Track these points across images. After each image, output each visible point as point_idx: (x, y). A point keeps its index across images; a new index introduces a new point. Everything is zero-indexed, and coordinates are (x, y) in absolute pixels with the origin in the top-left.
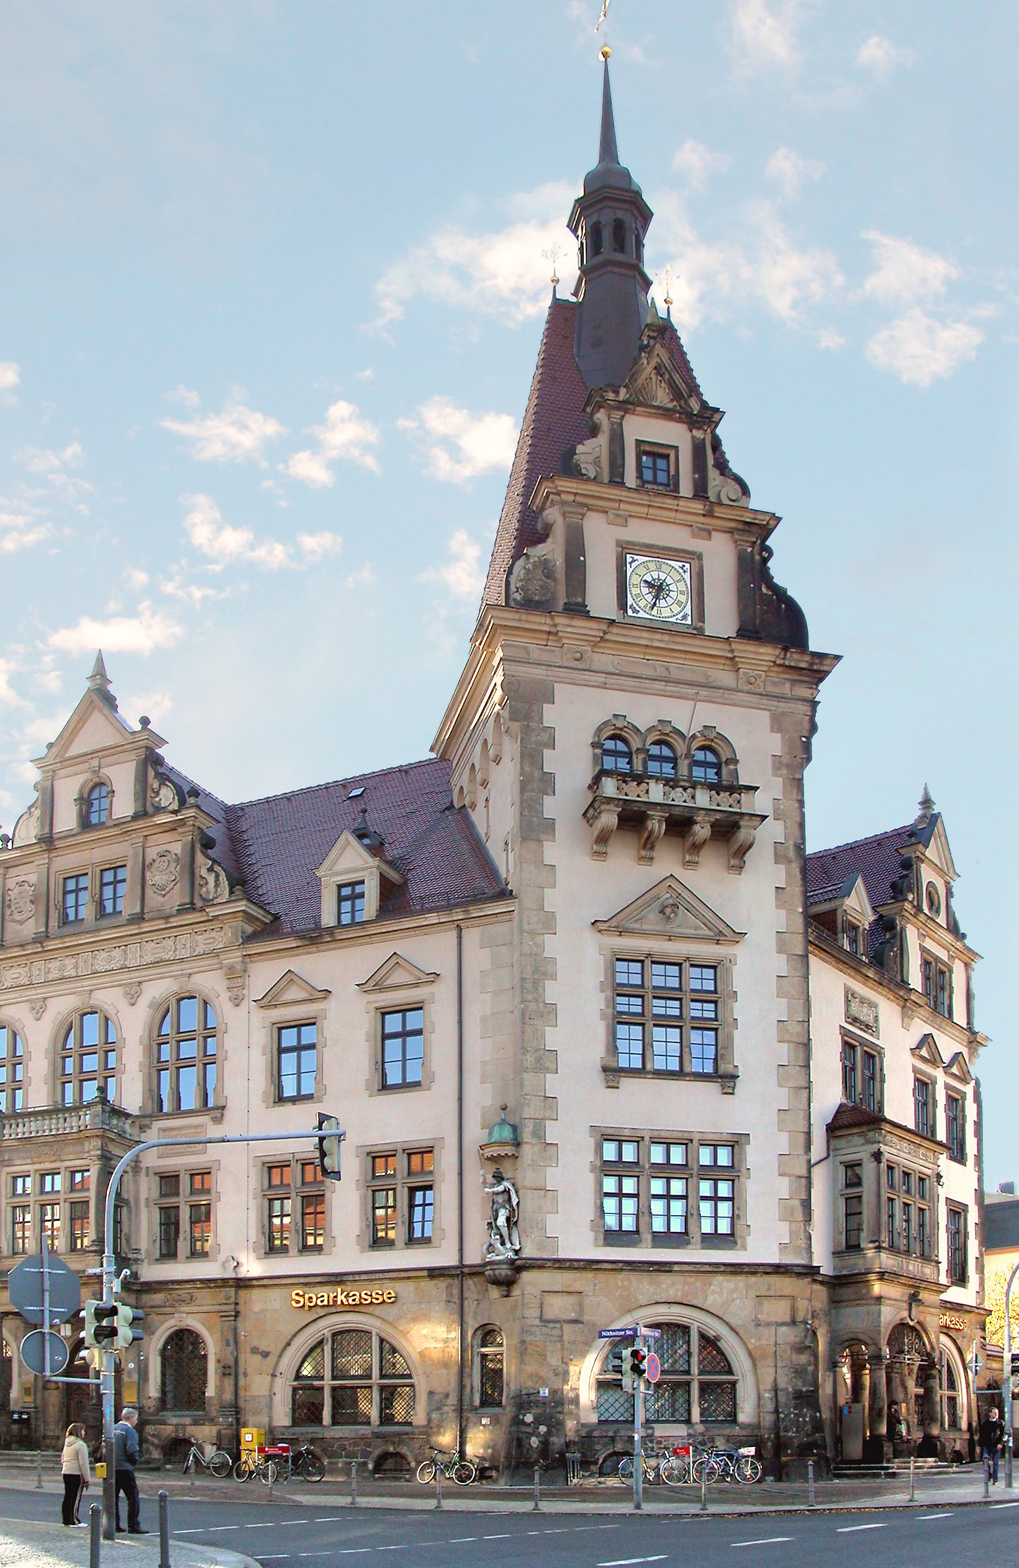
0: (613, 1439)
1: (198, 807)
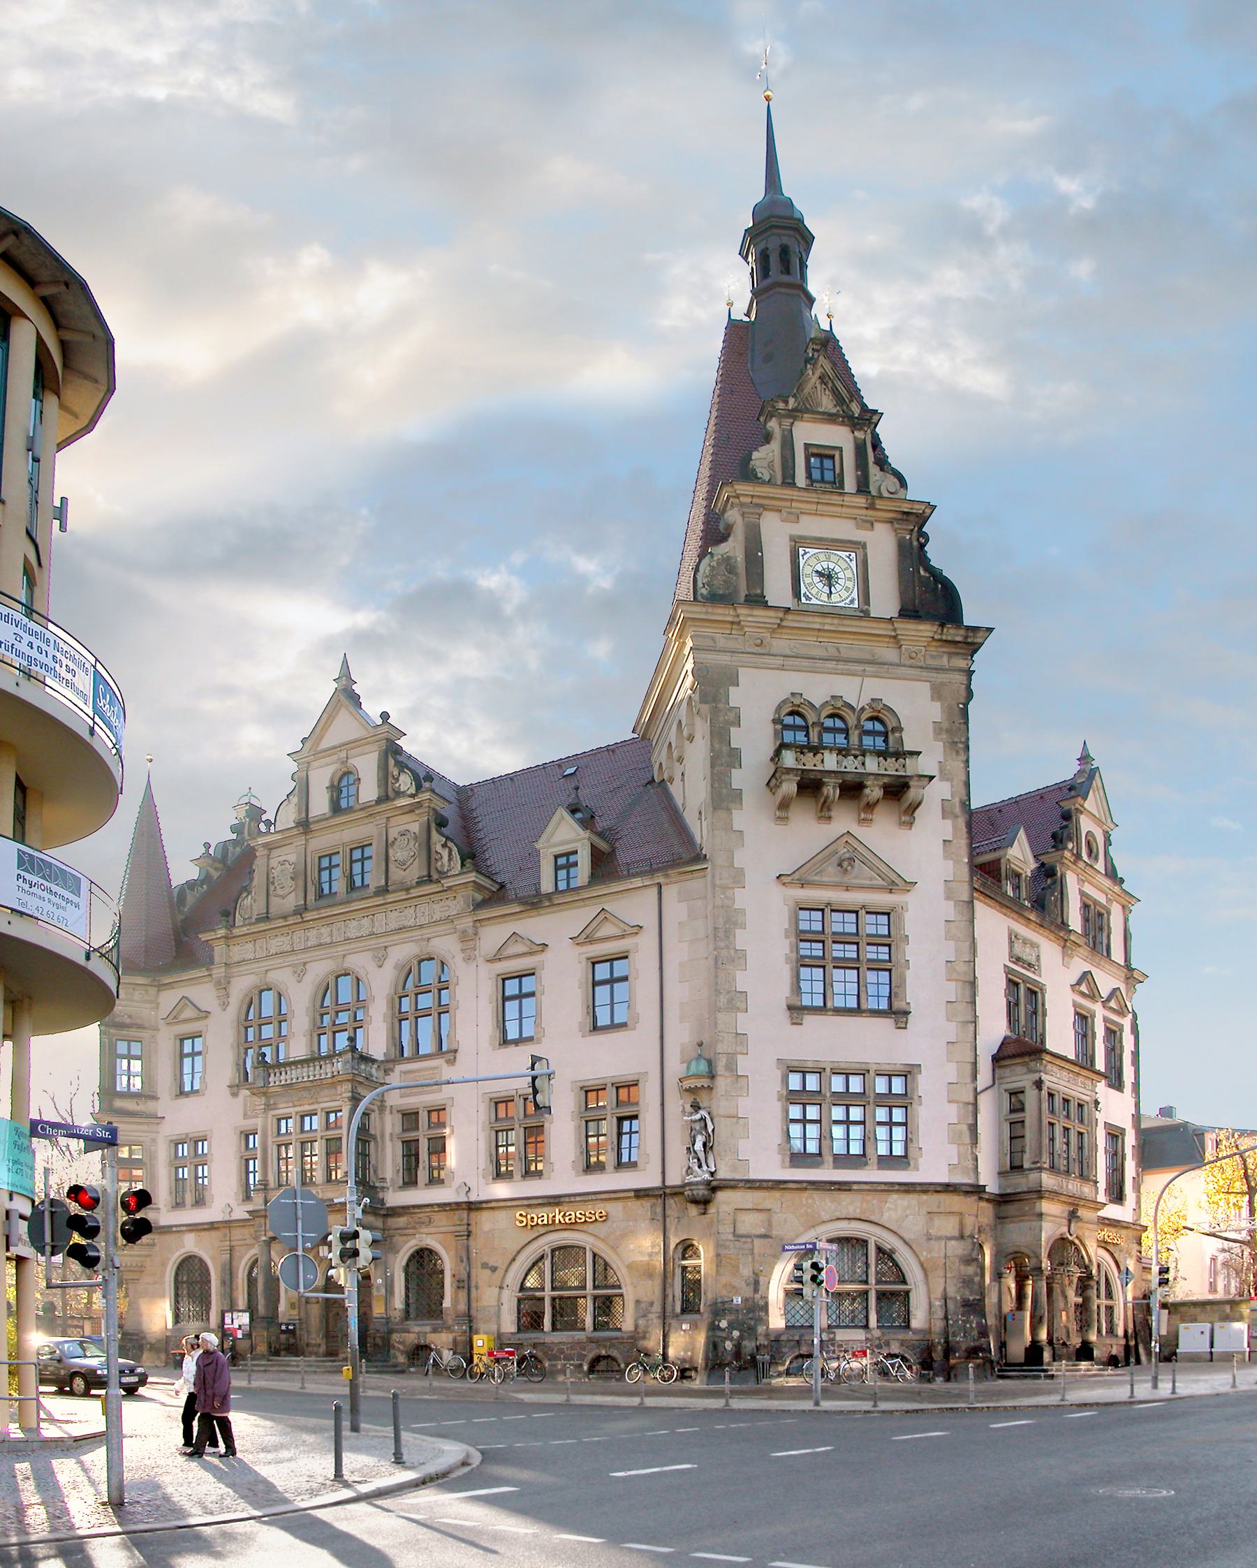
1: (433, 791)
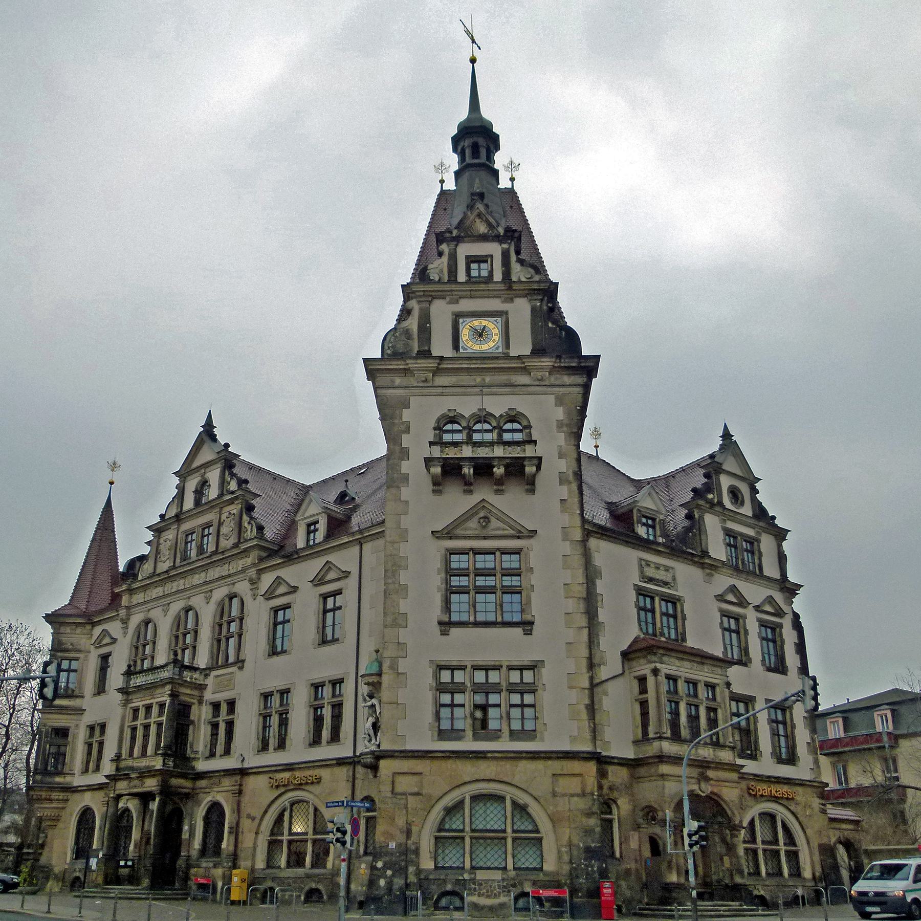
0: (445, 881)
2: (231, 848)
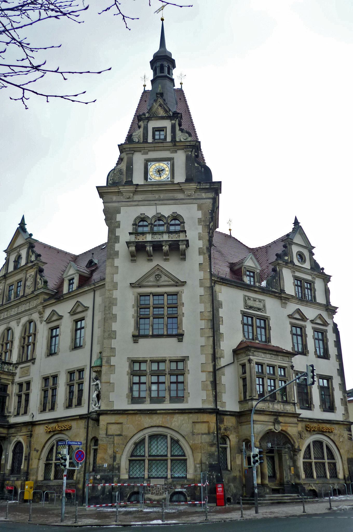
2: (26, 468)
